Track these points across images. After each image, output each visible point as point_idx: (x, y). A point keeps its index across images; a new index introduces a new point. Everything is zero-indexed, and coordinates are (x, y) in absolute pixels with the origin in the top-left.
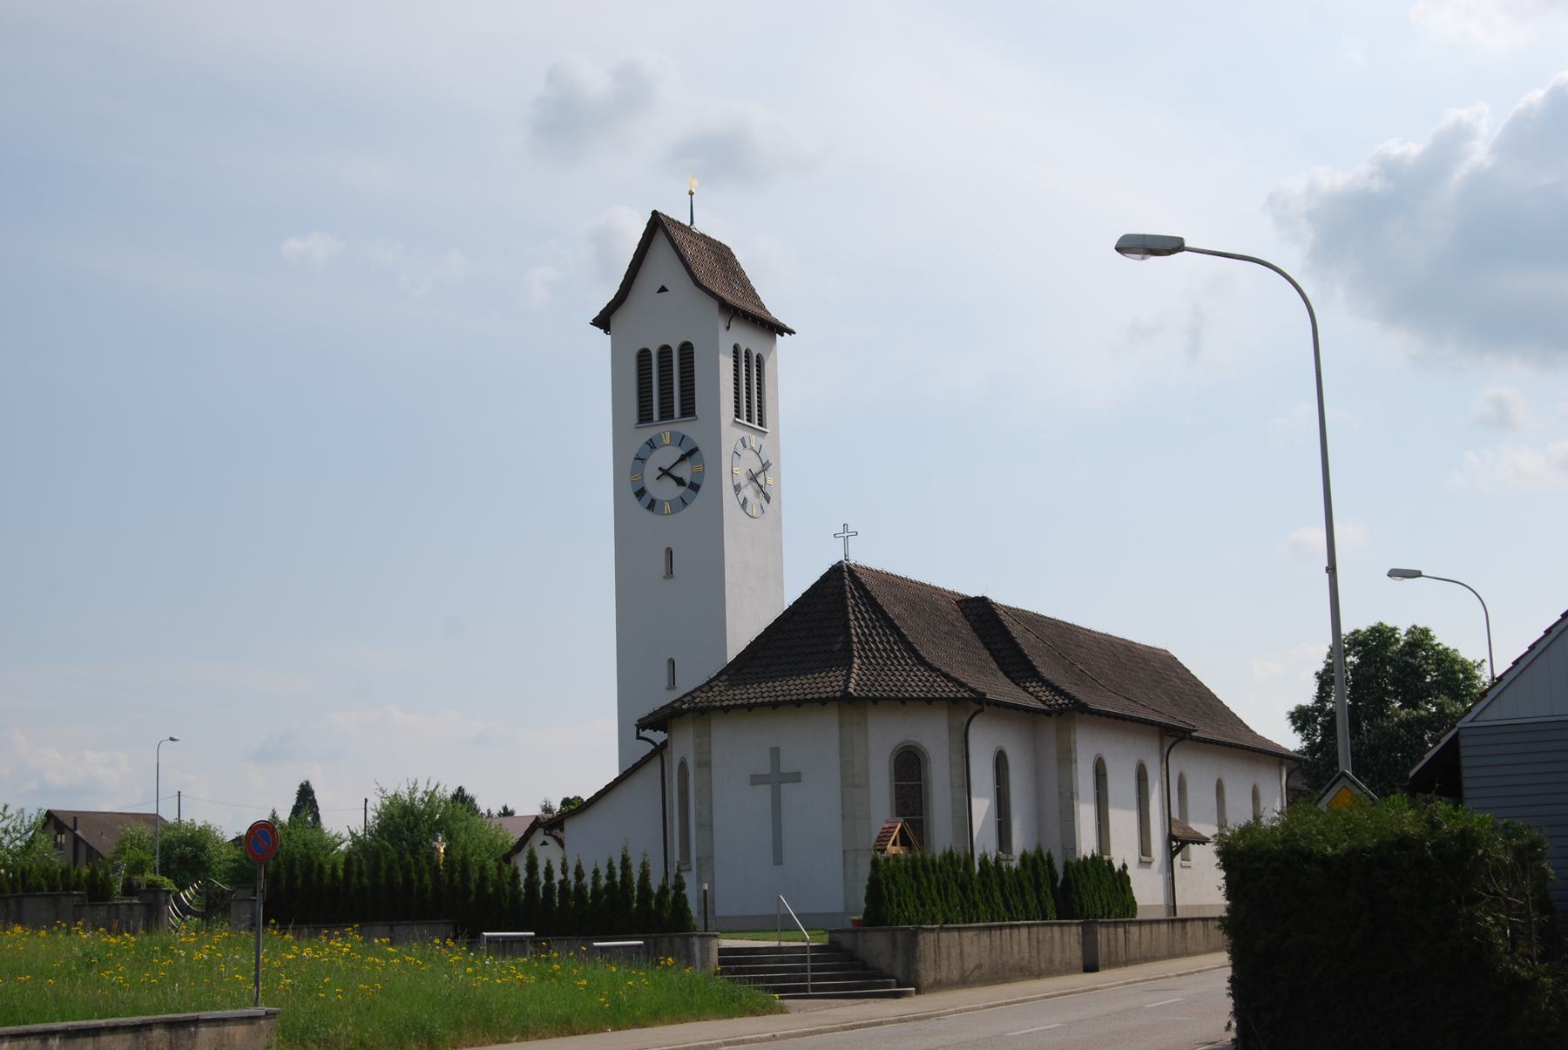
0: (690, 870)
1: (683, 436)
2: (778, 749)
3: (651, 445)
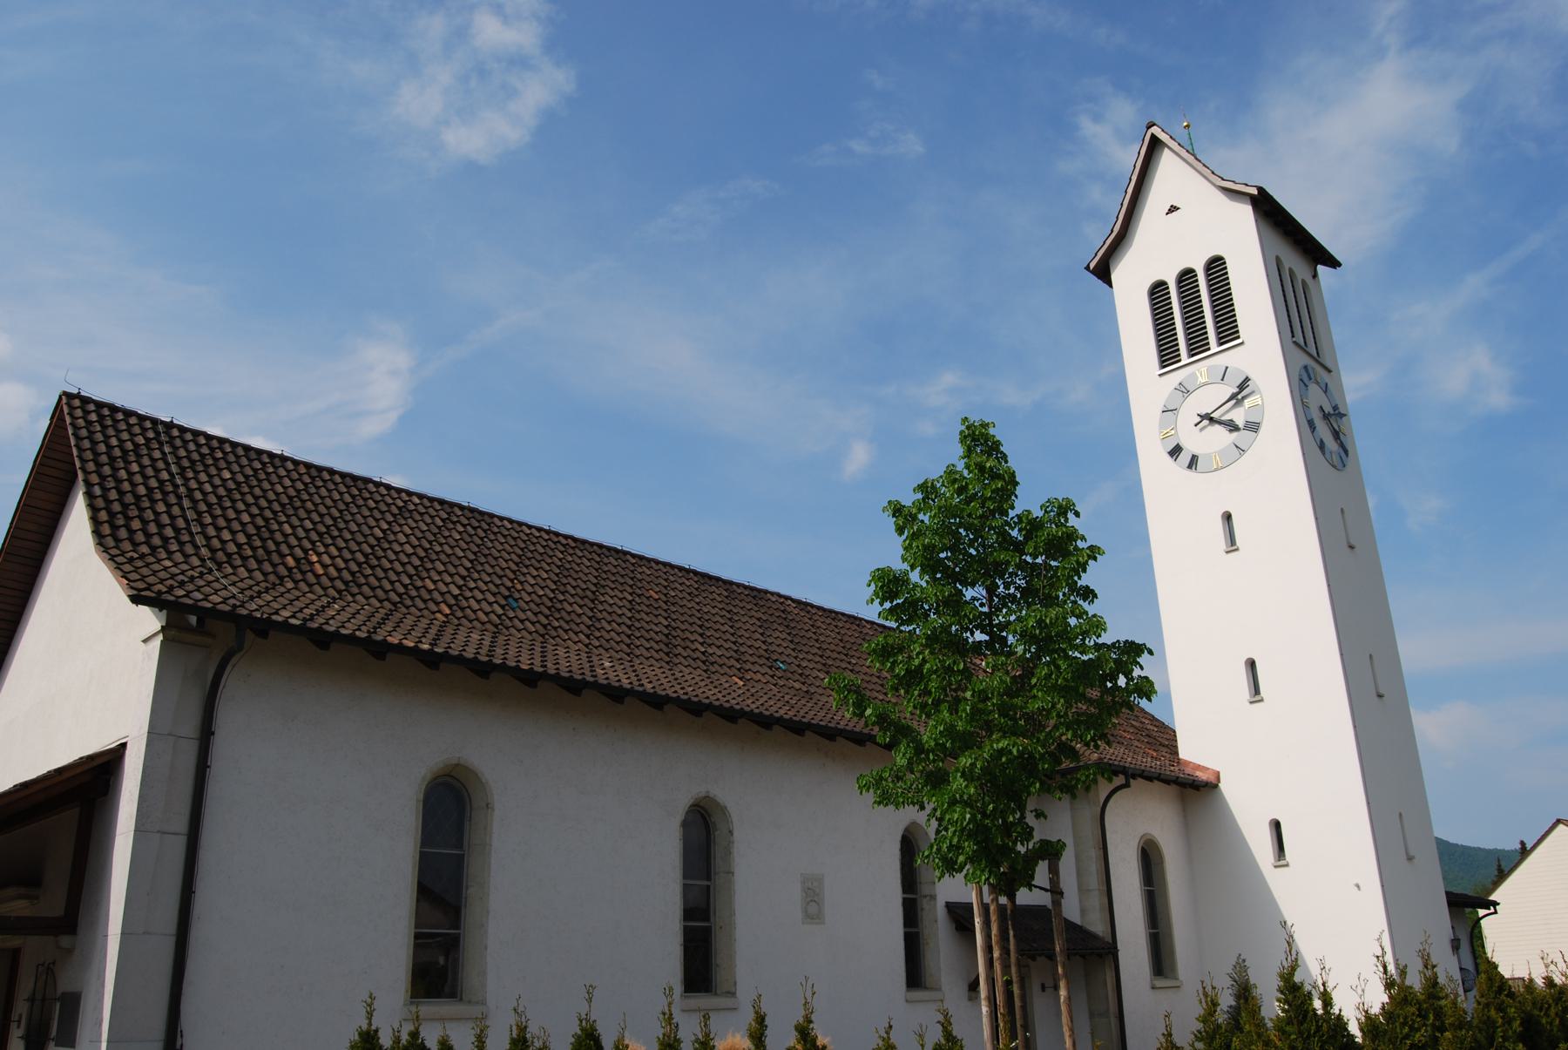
3: (1184, 390)
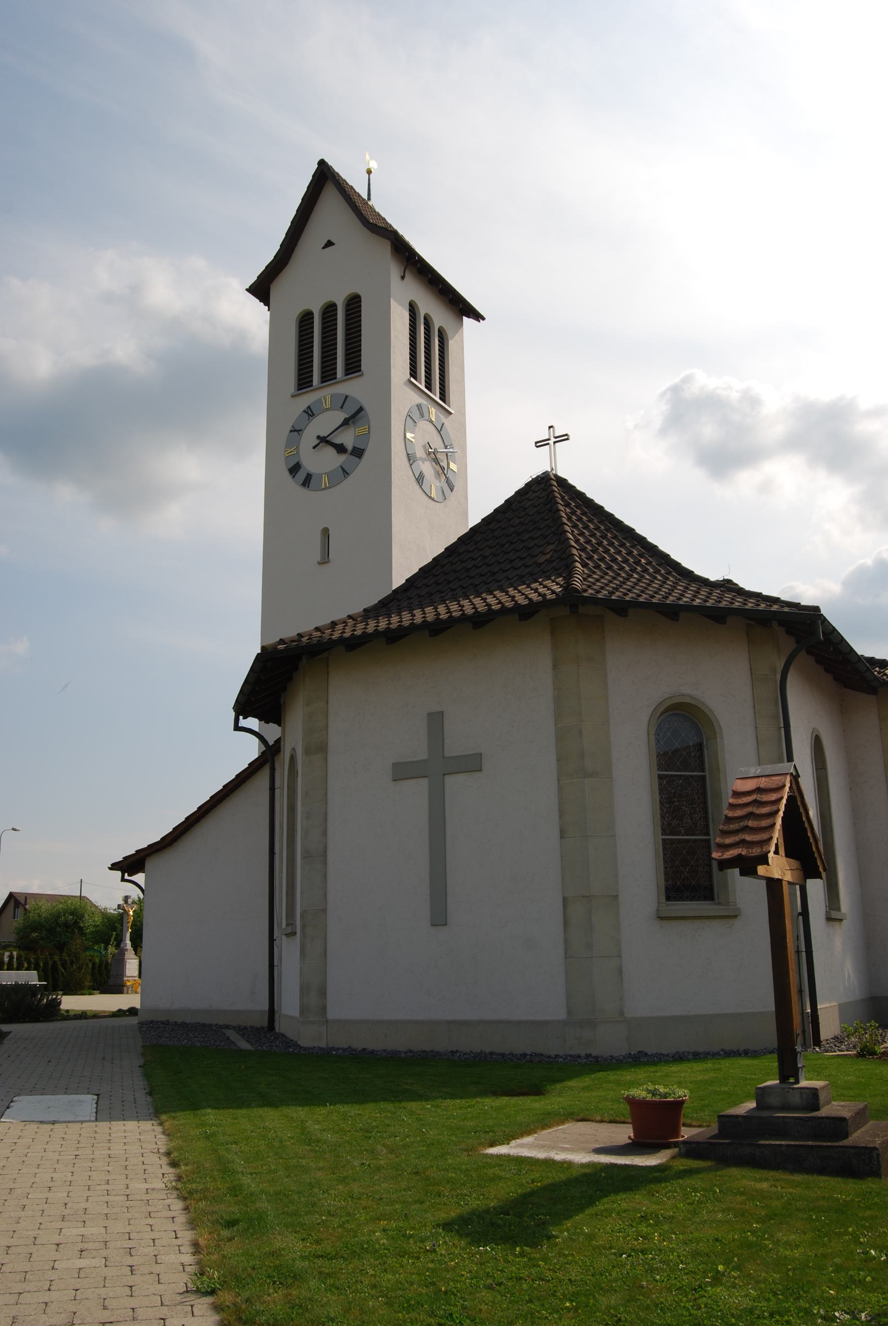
0: (295, 933)
1: (347, 397)
2: (442, 713)
3: (310, 413)
